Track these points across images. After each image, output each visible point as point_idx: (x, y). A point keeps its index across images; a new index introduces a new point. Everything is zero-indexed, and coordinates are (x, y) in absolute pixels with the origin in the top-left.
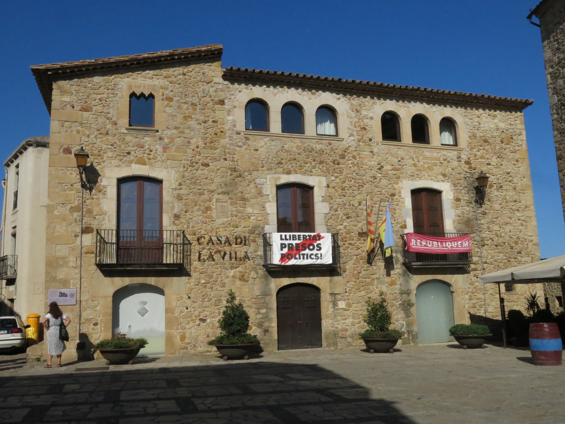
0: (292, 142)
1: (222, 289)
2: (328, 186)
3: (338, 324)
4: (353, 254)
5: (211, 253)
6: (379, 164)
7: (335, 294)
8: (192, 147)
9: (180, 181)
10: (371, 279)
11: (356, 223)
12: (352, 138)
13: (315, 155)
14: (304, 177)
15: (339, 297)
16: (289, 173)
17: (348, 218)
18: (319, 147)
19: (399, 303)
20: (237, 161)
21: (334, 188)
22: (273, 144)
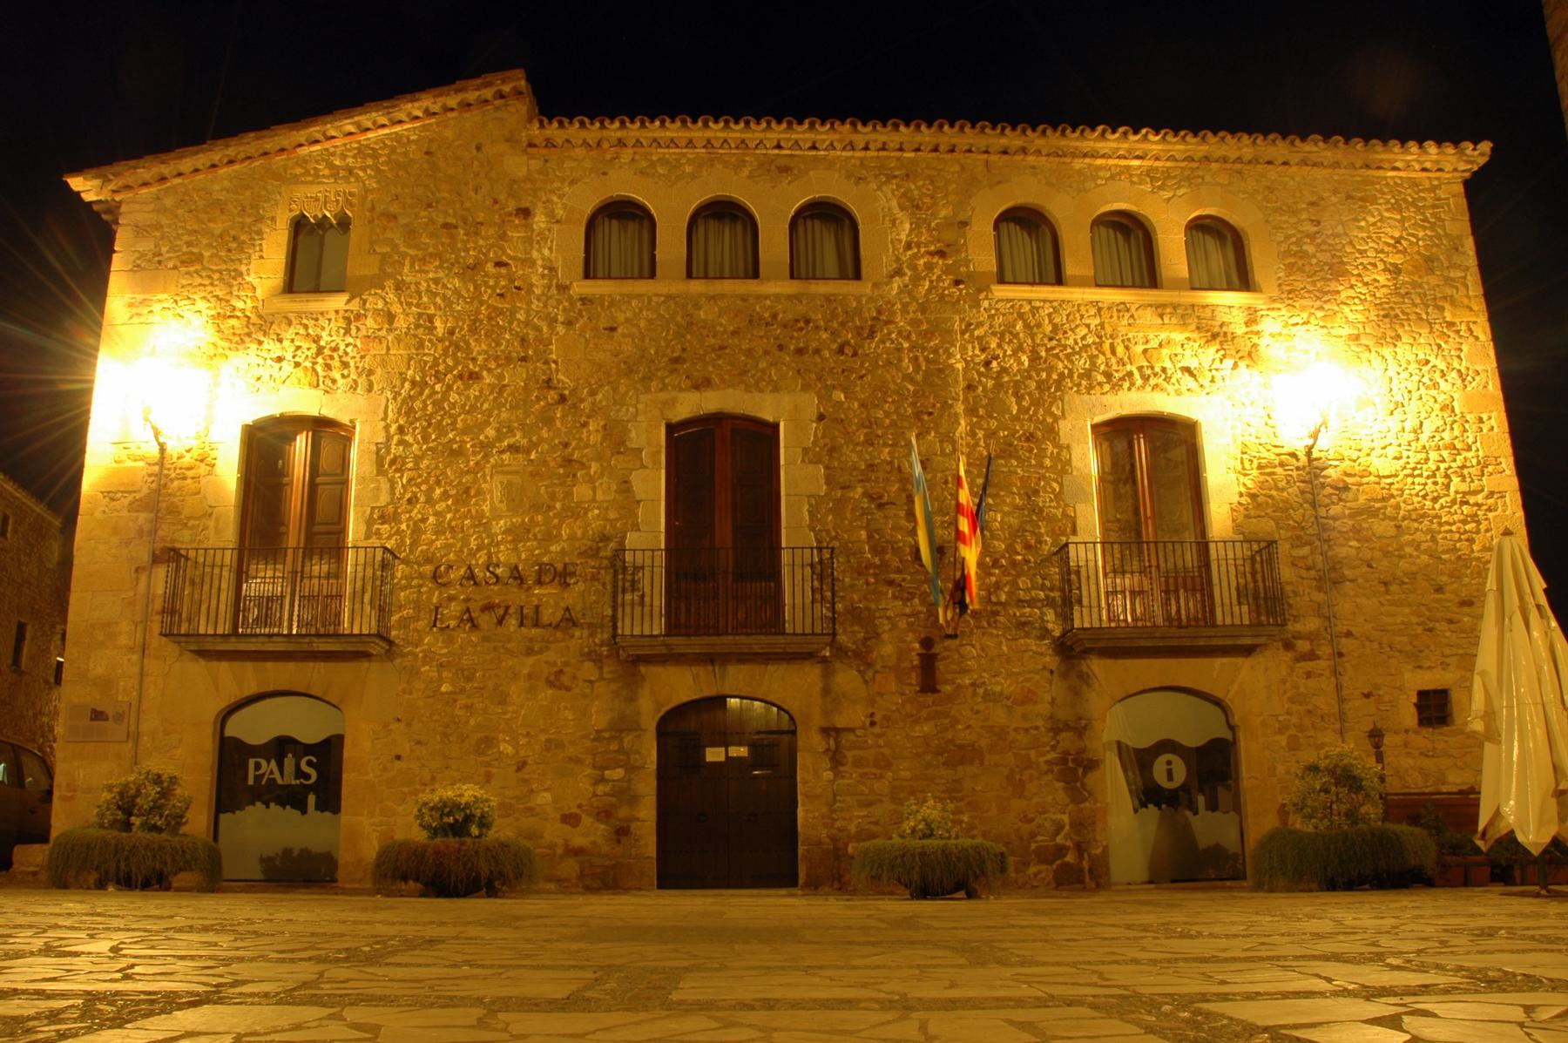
7: (838, 731)
14: (747, 396)
16: (702, 384)
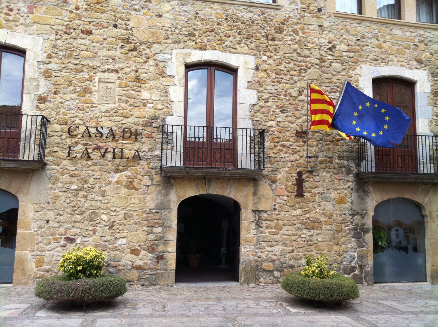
0: (211, 8)
1: (101, 198)
2: (257, 68)
3: (262, 252)
4: (287, 159)
5: (86, 149)
6: (330, 43)
7: (259, 211)
8: (70, 9)
9: (49, 52)
10: (310, 194)
11: (293, 119)
12: (293, 6)
13: (241, 26)
15: (265, 215)
17: (282, 112)
18: (247, 16)
19: (350, 227)
20: (131, 29)
21: (265, 71)
22: (184, 9)
